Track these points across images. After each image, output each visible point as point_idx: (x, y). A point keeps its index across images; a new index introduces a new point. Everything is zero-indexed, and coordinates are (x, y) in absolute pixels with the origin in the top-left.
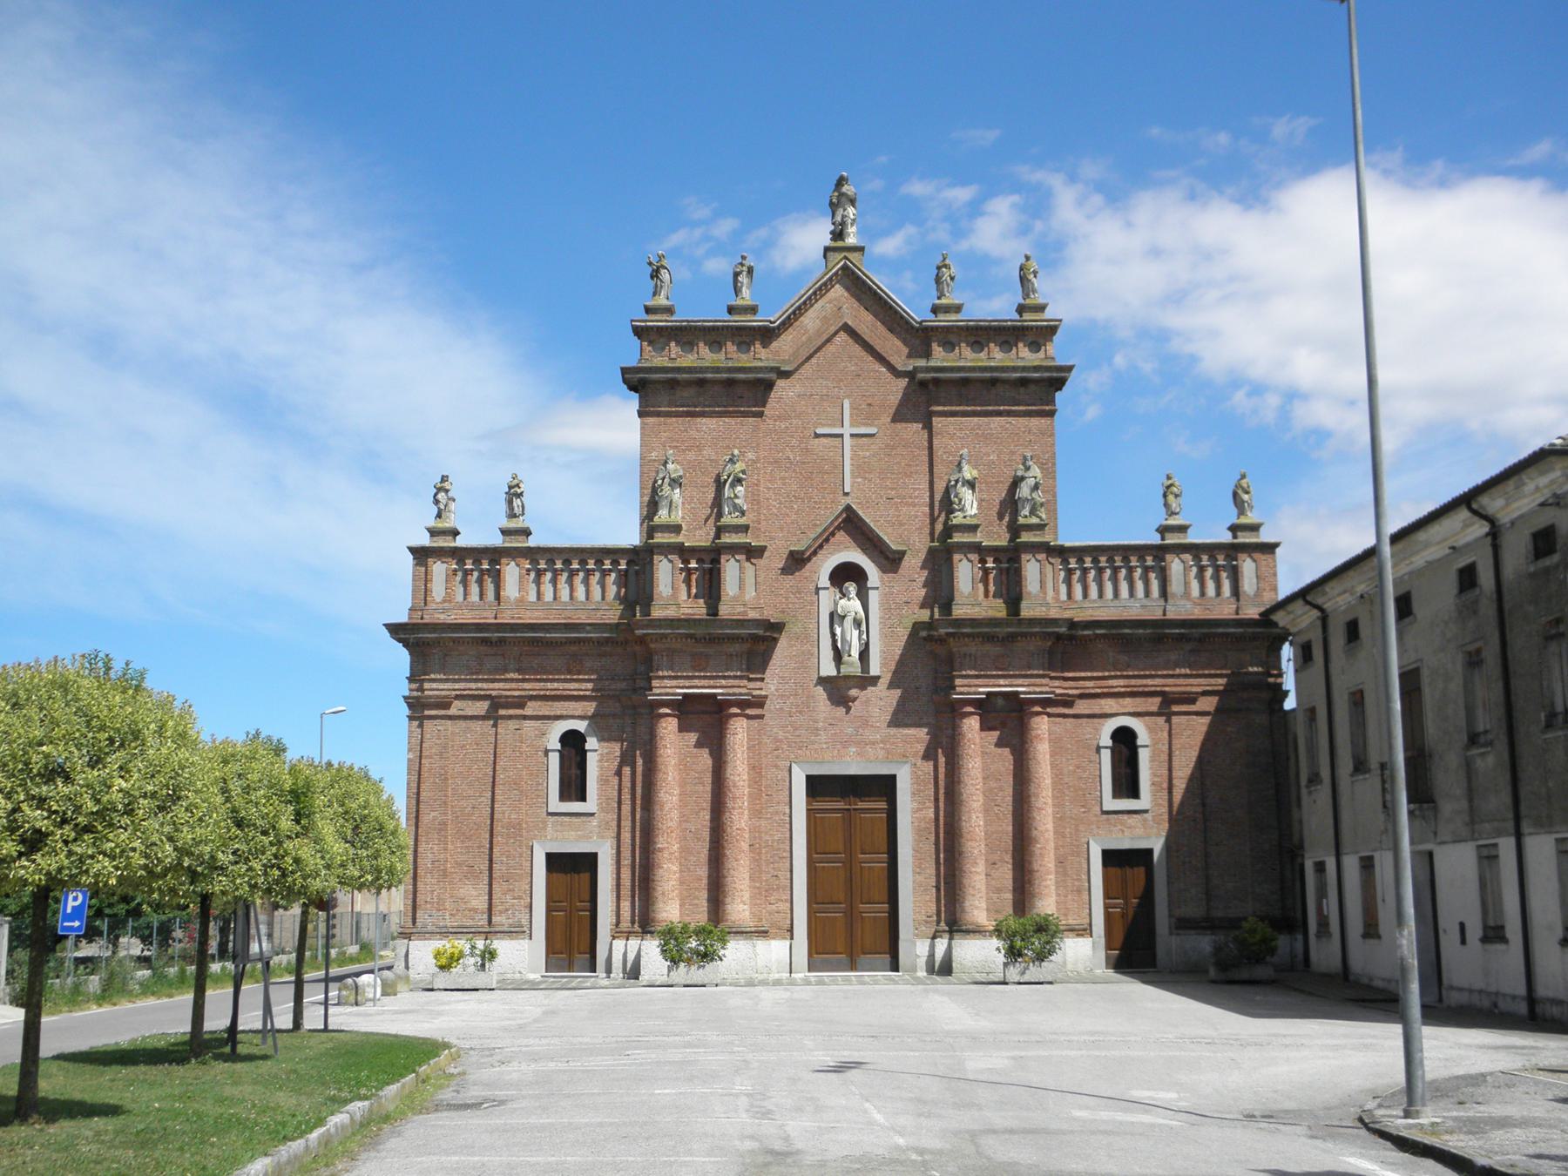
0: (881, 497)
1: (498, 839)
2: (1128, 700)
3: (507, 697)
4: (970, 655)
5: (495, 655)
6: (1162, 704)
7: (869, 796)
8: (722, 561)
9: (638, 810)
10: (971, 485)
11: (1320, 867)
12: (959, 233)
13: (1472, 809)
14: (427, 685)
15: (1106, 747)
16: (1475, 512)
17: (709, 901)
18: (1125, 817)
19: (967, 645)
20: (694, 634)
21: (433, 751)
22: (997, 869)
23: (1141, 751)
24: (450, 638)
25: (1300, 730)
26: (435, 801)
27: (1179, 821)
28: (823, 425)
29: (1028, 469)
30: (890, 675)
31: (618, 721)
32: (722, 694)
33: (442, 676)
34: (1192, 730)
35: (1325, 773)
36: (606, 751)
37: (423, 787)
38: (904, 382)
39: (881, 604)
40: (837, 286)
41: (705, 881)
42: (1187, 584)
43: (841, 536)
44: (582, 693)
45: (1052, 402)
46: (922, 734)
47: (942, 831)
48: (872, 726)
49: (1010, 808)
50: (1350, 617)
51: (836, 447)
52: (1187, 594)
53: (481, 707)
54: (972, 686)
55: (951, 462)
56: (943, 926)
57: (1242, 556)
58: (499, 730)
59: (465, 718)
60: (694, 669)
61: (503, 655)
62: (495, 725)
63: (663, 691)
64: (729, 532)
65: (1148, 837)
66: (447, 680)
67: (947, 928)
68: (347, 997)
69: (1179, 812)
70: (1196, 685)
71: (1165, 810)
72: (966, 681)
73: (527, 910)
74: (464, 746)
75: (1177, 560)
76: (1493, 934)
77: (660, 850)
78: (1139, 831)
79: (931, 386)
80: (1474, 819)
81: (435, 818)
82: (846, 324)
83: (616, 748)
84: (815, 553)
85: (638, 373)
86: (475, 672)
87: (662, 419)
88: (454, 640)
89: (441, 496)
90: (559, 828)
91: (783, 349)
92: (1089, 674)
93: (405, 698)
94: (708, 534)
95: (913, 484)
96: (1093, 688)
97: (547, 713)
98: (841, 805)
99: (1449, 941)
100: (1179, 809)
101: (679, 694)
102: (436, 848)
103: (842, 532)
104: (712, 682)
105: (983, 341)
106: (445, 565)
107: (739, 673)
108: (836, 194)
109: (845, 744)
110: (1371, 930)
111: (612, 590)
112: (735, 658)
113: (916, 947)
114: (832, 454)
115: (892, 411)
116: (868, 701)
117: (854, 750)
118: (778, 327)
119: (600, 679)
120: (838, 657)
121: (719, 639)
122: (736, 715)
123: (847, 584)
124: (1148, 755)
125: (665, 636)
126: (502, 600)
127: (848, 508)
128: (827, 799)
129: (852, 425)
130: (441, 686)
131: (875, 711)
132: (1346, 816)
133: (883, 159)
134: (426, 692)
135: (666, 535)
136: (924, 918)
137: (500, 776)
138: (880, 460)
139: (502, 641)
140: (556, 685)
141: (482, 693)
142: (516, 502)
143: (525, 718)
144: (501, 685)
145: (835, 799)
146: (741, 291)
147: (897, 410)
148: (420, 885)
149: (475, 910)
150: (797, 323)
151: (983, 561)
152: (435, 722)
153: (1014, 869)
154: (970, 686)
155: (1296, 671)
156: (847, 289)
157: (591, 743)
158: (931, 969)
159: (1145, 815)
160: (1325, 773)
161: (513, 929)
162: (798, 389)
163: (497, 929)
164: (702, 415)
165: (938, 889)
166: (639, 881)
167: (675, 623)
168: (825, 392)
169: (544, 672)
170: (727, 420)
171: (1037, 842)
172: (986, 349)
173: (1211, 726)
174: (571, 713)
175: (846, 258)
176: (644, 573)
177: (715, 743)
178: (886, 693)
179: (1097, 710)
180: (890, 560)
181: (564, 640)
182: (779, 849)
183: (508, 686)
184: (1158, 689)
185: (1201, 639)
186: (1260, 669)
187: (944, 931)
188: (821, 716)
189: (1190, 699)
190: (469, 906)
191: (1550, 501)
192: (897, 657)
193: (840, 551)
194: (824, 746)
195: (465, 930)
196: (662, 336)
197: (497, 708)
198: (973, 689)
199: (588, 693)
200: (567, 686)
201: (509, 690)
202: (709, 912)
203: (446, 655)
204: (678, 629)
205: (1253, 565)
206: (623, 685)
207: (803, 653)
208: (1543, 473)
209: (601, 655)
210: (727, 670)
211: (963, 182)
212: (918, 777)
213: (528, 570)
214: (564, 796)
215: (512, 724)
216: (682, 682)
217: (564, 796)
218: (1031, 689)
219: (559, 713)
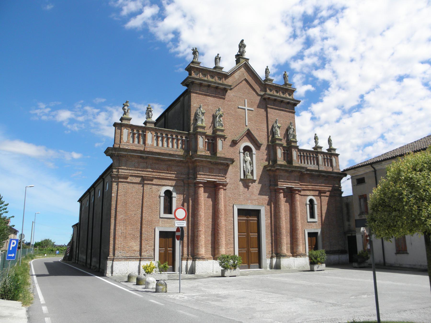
1: (144, 226)
2: (312, 192)
3: (148, 177)
4: (282, 176)
5: (144, 162)
6: (319, 193)
7: (252, 216)
8: (217, 140)
9: (190, 217)
10: (279, 127)
12: (94, 118)
14: (120, 171)
15: (308, 204)
17: (211, 248)
18: (312, 223)
19: (281, 172)
20: (211, 161)
24: (130, 155)
26: (122, 211)
27: (324, 225)
30: (258, 180)
31: (182, 188)
32: (218, 181)
33: (125, 168)
34: (325, 200)
36: (178, 198)
37: (118, 206)
38: (259, 98)
40: (243, 68)
41: (210, 241)
43: (245, 138)
44: (171, 178)
45: (294, 110)
46: (266, 198)
47: (273, 226)
48: (254, 195)
49: (289, 220)
51: (243, 112)
53: (138, 180)
54: (283, 185)
55: (272, 121)
56: (274, 255)
58: (145, 188)
59: (133, 183)
60: (209, 172)
61: (146, 163)
62: (143, 186)
64: (219, 131)
65: (317, 229)
66: (127, 169)
67: (275, 255)
68: (163, 289)
69: (324, 222)
70: (327, 189)
71: (320, 222)
73: (153, 251)
74: (132, 193)
77: (200, 231)
78: (315, 227)
79: (267, 100)
81: (122, 218)
83: (182, 197)
85: (193, 79)
86: (136, 168)
87: (197, 95)
88: (131, 156)
89: (126, 107)
90: (164, 223)
91: (229, 81)
92: (304, 184)
94: (211, 132)
95: (263, 126)
96: (305, 188)
97: (160, 184)
98: (245, 218)
100: (324, 221)
102: (122, 228)
103: (246, 137)
104: (215, 177)
105: (278, 91)
106: (127, 130)
107: (223, 175)
108: (241, 44)
109: (248, 200)
111: (180, 146)
113: (266, 261)
114: (242, 114)
115: (257, 105)
116: (253, 187)
118: (229, 75)
119: (177, 174)
121: (218, 164)
122: (222, 188)
125: (202, 161)
126: (146, 144)
127: (248, 130)
128: (241, 216)
129: (247, 107)
130: (125, 171)
131: (255, 190)
133: (82, 101)
134: (120, 173)
135: (201, 129)
136: (268, 252)
137: (145, 204)
138: (254, 118)
139: (147, 158)
140: (163, 174)
141: (139, 175)
142: (150, 113)
143: (153, 184)
144: (145, 173)
145: (243, 216)
146: (217, 63)
147: (258, 104)
148: (117, 242)
149: (135, 251)
150: (233, 76)
152: (123, 184)
153: (290, 238)
154: (281, 184)
156: (245, 69)
157: (174, 194)
158: (271, 268)
159: (316, 223)
161: (150, 257)
162: (233, 94)
163: (144, 257)
164: (209, 96)
165: (272, 244)
166: (191, 241)
167: (207, 157)
168: (240, 96)
169: (159, 170)
170: (215, 99)
171: (298, 230)
172: (279, 93)
173: (329, 200)
175: (246, 61)
177: (214, 197)
178: (258, 185)
179: (305, 194)
180: (258, 146)
181: (167, 160)
182: (230, 231)
183: (148, 173)
184: (318, 189)
185: (327, 177)
186: (338, 186)
187: (275, 256)
188: (241, 191)
189: (325, 192)
190: (133, 249)
192: (260, 175)
193: (245, 142)
195: (132, 258)
196: (197, 71)
197: (144, 180)
198: (282, 185)
199: (173, 178)
200: (167, 175)
201: (148, 175)
202: (211, 251)
203: (127, 161)
204: (208, 159)
206: (184, 176)
207: (236, 171)
209: (177, 166)
210: (219, 174)
211: (97, 108)
212: (266, 210)
213: (155, 136)
214: (165, 212)
215: (149, 186)
216: (206, 176)
217: (165, 212)
218: (296, 186)
219: (164, 184)
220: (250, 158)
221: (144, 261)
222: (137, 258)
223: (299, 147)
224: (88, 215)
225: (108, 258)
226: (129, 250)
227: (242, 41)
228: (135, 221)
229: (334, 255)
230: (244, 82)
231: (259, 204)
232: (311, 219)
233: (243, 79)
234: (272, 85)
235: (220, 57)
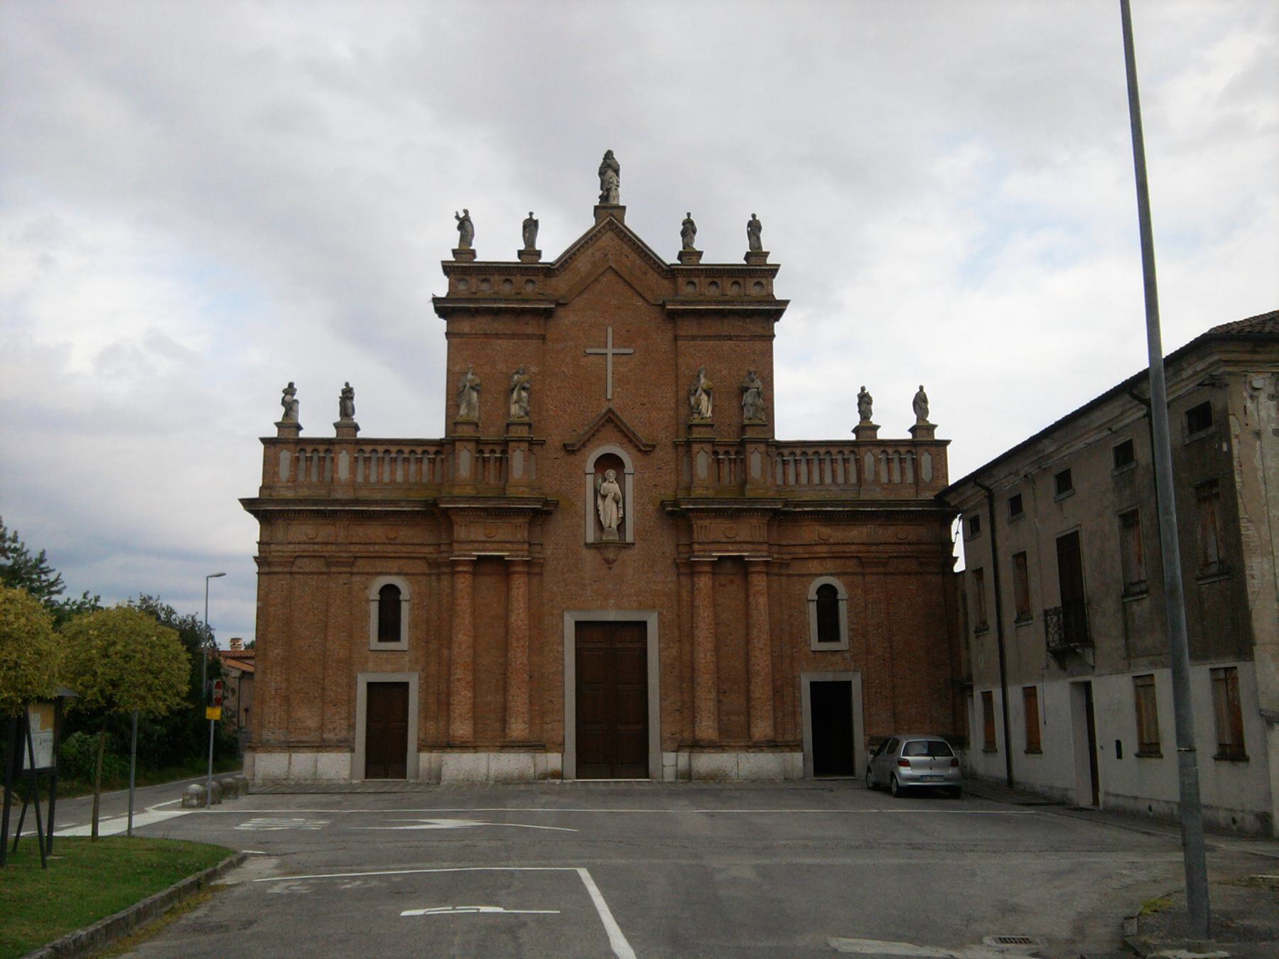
0: (636, 403)
11: (987, 697)
13: (1127, 648)
15: (813, 601)
16: (1135, 397)
21: (278, 600)
23: (840, 602)
25: (970, 587)
28: (591, 347)
29: (753, 381)
35: (992, 622)
39: (635, 487)
50: (1014, 494)
57: (920, 450)
76: (1149, 749)
80: (1130, 655)
82: (610, 267)
84: (584, 445)
99: (1106, 757)
101: (474, 556)
102: (279, 678)
110: (1033, 747)
118: (557, 269)
120: (600, 525)
123: (607, 471)
124: (846, 607)
129: (613, 347)
132: (1009, 655)
151: (715, 453)
155: (965, 541)
160: (992, 622)
174: (388, 571)
175: (611, 215)
191: (1206, 382)
205: (930, 457)
208: (1201, 359)
212: (664, 623)
214: (382, 638)
217: (382, 638)
218: (753, 554)
219: (379, 570)
220: (617, 485)
221: (327, 752)
222: (312, 747)
224: (998, 667)
226: (296, 729)
227: (609, 155)
231: (641, 607)
233: (606, 267)
234: (712, 269)
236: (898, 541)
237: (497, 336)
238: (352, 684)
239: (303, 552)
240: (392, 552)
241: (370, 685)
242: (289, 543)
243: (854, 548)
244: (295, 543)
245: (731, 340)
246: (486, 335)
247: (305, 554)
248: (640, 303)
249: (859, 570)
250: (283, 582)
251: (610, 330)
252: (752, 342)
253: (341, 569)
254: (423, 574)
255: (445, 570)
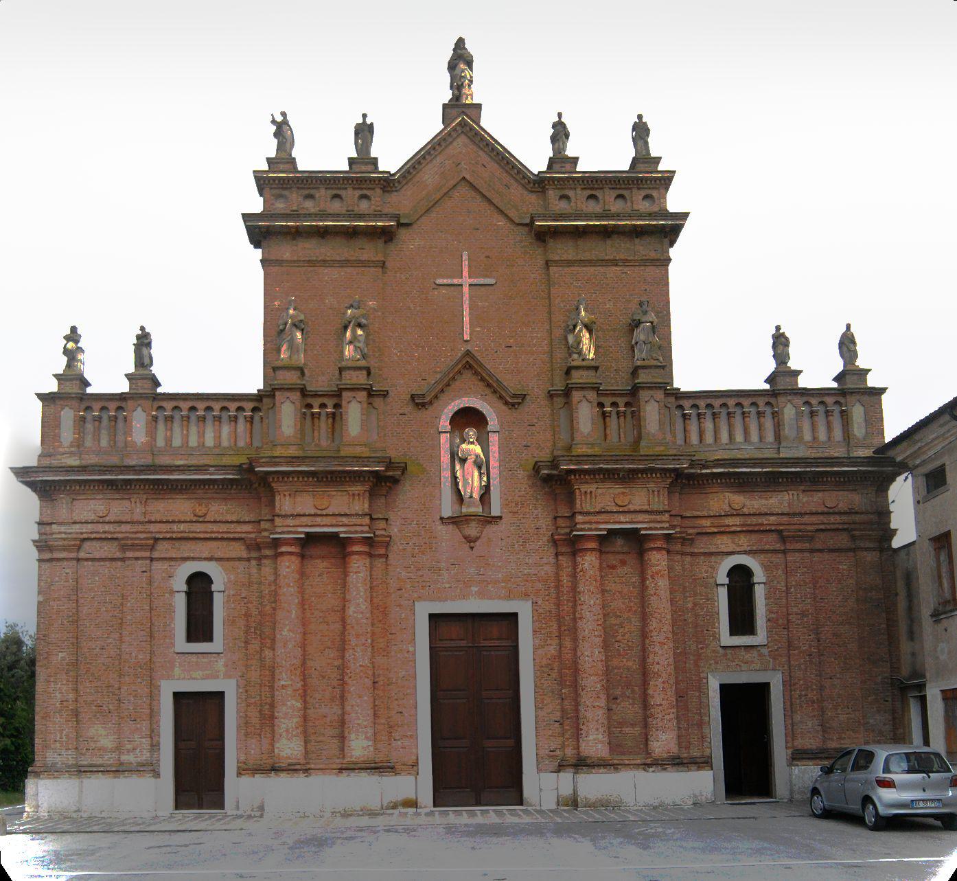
22: (619, 704)
28: (443, 277)
42: (799, 429)
52: (799, 438)
63: (286, 529)
72: (587, 518)
75: (789, 406)
81: (63, 659)
82: (464, 178)
93: (34, 541)
102: (65, 688)
112: (356, 498)
117: (476, 589)
149: (104, 749)
174: (198, 556)
176: (268, 418)
190: (98, 745)
194: (447, 586)
198: (594, 526)
205: (862, 408)
212: (540, 615)
223: (869, 376)
225: (30, 769)
228: (104, 668)
229: (678, 771)
230: (464, 190)
232: (759, 632)
235: (372, 124)
236: (826, 510)
237: (324, 263)
238: (153, 693)
239: (91, 533)
240: (200, 532)
241: (177, 695)
242: (75, 523)
243: (773, 519)
244: (82, 523)
245: (617, 265)
246: (311, 263)
247: (93, 536)
248: (502, 222)
249: (778, 546)
250: (67, 571)
251: (465, 257)
252: (643, 268)
253: (138, 554)
254: (240, 559)
255: (268, 552)
